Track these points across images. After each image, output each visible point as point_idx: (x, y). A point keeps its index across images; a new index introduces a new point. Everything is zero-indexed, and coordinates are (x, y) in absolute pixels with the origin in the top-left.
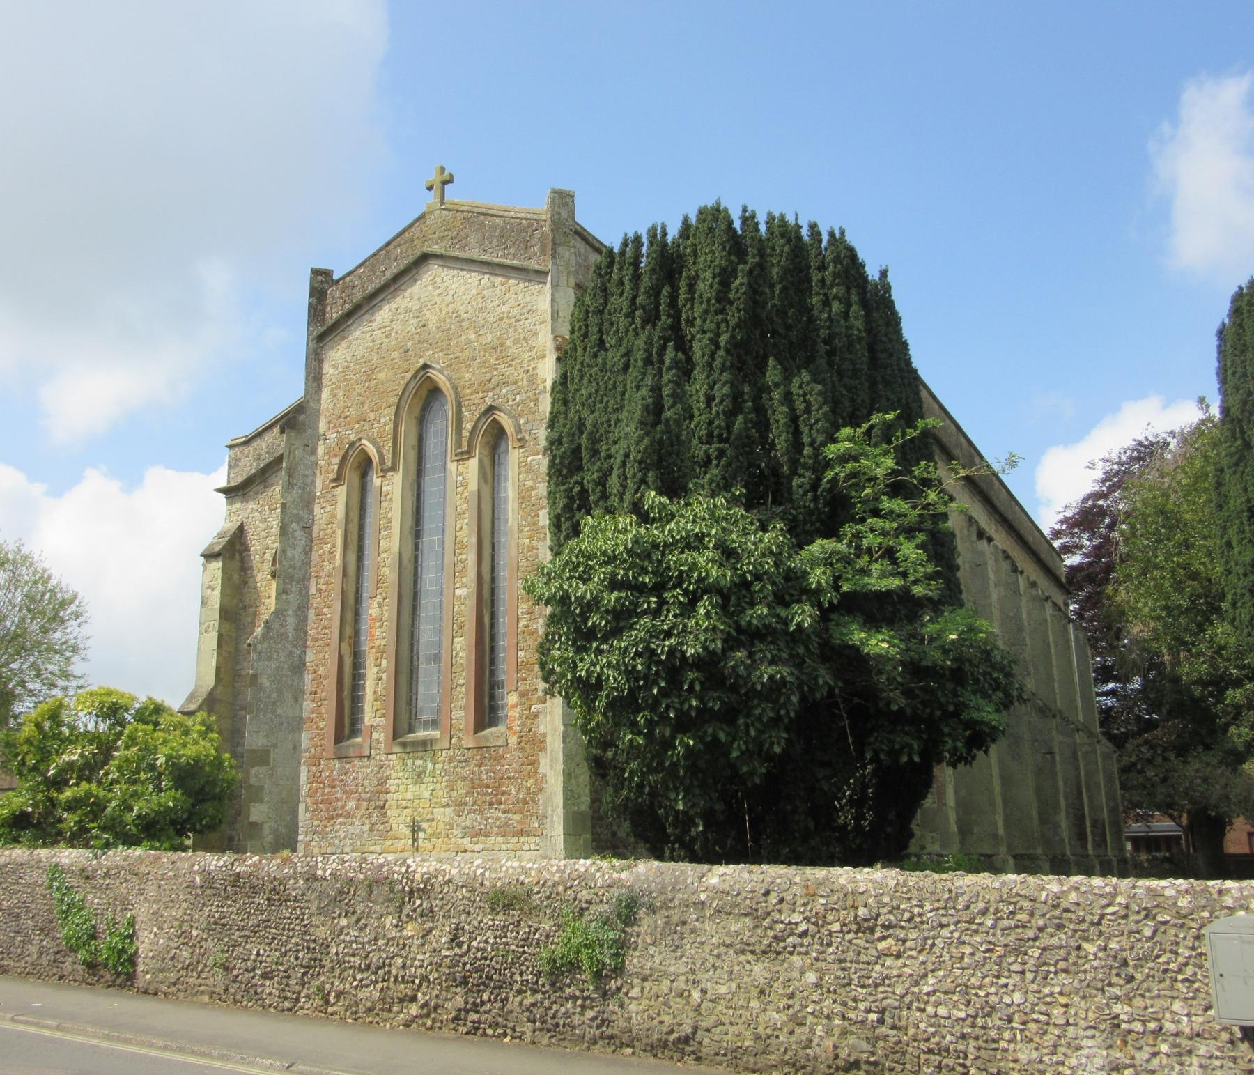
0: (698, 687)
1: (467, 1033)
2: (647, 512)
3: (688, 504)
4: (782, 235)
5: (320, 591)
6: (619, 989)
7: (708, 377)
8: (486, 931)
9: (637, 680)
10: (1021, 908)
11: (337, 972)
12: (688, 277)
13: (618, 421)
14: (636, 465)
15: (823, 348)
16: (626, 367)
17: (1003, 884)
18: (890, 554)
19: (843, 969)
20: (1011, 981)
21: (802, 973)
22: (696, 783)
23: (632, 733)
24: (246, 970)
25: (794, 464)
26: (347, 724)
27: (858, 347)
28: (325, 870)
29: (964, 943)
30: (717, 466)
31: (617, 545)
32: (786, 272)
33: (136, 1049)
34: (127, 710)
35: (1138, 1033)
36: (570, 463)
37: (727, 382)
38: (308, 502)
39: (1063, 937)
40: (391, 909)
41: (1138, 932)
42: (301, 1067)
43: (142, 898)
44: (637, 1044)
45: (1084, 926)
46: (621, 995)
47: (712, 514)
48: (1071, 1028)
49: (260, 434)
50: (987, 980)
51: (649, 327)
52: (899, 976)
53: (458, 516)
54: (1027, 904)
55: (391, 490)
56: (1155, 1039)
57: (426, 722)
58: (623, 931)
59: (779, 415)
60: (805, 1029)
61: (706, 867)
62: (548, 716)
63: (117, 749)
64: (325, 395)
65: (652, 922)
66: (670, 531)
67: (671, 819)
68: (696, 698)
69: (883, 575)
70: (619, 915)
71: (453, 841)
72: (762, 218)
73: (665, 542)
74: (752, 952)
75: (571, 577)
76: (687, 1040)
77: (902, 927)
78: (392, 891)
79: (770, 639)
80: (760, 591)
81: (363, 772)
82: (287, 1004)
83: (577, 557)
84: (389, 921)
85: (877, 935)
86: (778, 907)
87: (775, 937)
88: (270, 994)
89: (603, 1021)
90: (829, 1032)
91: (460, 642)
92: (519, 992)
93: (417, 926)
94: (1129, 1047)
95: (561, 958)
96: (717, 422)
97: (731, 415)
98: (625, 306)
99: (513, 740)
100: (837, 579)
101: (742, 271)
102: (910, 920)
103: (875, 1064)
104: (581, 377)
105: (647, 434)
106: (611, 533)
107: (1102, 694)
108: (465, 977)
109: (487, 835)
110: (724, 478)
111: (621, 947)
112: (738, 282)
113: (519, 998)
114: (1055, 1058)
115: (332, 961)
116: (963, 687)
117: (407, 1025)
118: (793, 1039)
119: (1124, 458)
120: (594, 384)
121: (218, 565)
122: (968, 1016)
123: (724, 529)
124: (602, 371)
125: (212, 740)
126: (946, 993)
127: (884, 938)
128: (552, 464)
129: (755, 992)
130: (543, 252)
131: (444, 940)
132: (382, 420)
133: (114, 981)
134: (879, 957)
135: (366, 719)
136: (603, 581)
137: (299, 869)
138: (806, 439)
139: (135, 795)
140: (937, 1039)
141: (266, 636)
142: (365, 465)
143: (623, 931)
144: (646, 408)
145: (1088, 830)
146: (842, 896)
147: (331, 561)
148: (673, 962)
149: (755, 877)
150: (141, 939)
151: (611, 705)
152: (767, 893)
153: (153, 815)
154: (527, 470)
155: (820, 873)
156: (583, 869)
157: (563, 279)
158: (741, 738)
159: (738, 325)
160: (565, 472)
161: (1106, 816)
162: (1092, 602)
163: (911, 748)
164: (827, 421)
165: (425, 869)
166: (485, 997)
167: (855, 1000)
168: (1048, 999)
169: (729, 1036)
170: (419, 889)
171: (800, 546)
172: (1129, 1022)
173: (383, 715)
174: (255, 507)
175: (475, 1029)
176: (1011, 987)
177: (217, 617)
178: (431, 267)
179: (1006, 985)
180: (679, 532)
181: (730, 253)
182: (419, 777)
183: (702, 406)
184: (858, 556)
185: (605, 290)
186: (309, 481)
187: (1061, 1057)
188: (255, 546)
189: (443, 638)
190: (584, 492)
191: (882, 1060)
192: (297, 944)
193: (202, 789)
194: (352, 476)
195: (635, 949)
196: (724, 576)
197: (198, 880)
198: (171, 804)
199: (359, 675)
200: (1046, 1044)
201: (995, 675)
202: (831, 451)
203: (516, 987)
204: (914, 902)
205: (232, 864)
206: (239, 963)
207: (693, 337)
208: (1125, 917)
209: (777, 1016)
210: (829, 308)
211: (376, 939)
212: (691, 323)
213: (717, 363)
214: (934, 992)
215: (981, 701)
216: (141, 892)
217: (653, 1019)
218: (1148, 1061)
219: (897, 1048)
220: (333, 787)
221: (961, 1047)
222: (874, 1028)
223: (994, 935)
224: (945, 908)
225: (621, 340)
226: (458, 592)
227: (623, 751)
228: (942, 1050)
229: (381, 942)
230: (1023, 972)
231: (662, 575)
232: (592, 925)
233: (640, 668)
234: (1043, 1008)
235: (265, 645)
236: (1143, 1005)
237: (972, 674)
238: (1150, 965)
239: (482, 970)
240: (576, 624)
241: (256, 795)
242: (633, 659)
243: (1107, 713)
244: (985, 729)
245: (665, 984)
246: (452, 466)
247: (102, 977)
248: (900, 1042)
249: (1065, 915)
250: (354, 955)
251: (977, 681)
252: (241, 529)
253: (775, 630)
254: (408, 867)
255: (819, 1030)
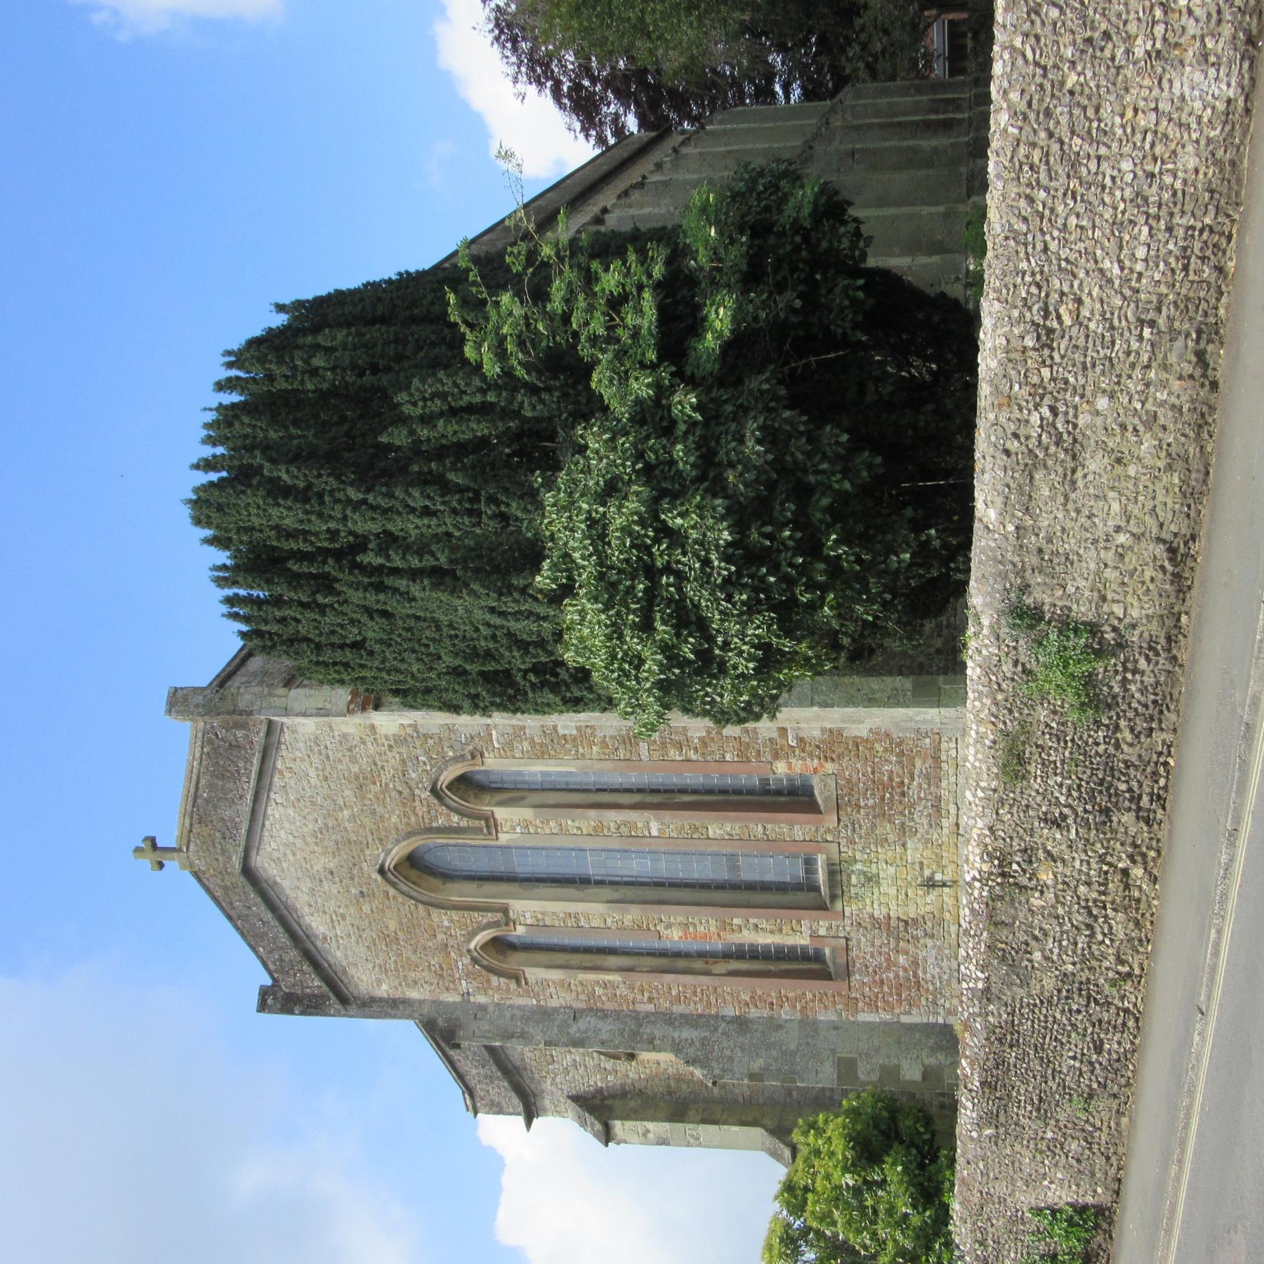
0: (769, 529)
1: (1164, 808)
2: (561, 586)
3: (552, 538)
4: (230, 425)
5: (650, 1000)
6: (1115, 629)
7: (399, 514)
8: (1049, 786)
9: (759, 602)
10: (1027, 157)
11: (1095, 963)
12: (278, 539)
13: (451, 625)
14: (503, 599)
15: (368, 379)
16: (385, 614)
17: (998, 176)
18: (616, 303)
19: (1094, 366)
20: (1109, 172)
21: (1098, 413)
22: (880, 537)
23: (822, 607)
24: (1092, 1072)
25: (506, 414)
26: (808, 965)
27: (368, 336)
28: (977, 979)
29: (1065, 225)
30: (508, 505)
31: (599, 623)
32: (274, 420)
33: (1183, 1195)
34: (789, 1225)
35: (1166, 30)
36: (500, 684)
37: (407, 492)
38: (544, 1015)
39: (1059, 109)
40: (1023, 899)
41: (1055, 24)
42: (1202, 998)
43: (1009, 1200)
44: (1176, 609)
45: (1048, 86)
46: (1121, 627)
47: (565, 508)
48: (1160, 106)
49: (460, 1077)
50: (1107, 200)
51: (337, 586)
52: (1102, 301)
53: (563, 831)
54: (1022, 150)
55: (530, 912)
56: (1173, 10)
57: (807, 871)
58: (1049, 623)
59: (449, 430)
60: (1160, 412)
61: (976, 525)
62: (803, 725)
63: (836, 1235)
64: (414, 994)
65: (1039, 589)
66: (583, 558)
67: (921, 571)
68: (782, 531)
69: (639, 312)
70: (1031, 627)
71: (945, 839)
72: (208, 451)
73: (597, 564)
74: (1074, 471)
75: (637, 678)
76: (1172, 551)
77: (1047, 295)
78: (1002, 898)
79: (713, 444)
80: (656, 453)
81: (865, 947)
82: (1131, 1023)
83: (613, 671)
84: (1036, 902)
85: (1055, 325)
86: (1022, 439)
87: (1057, 444)
88: (1119, 1043)
89: (1150, 648)
90: (1164, 385)
91: (714, 831)
92: (1117, 746)
93: (1042, 868)
94: (1182, 41)
95: (1079, 696)
96: (455, 504)
97: (447, 488)
98: (311, 615)
99: (830, 767)
100: (643, 366)
101: (271, 471)
102: (1039, 287)
103: (1199, 332)
104: (398, 671)
105: (467, 585)
106: (585, 631)
107: (787, 98)
108: (1101, 811)
109: (939, 798)
110: (522, 497)
111: (1067, 626)
112: (284, 476)
113: (1125, 747)
114: (1194, 126)
115: (1082, 970)
116: (773, 224)
117: (1155, 880)
118: (1171, 427)
119: (514, 59)
120: (406, 655)
121: (618, 1126)
122: (1146, 223)
123: (582, 495)
124: (390, 645)
125: (826, 1122)
126: (1121, 248)
127: (1059, 317)
128: (502, 707)
129: (1119, 469)
130: (243, 726)
131: (1058, 836)
132: (446, 923)
133: (1105, 1231)
134: (1081, 324)
135: (803, 942)
136: (642, 640)
137: (977, 1010)
138: (478, 399)
139: (891, 1211)
140: (1172, 260)
141: (704, 1064)
142: (500, 945)
143: (1049, 623)
144: (435, 586)
145: (941, 117)
146: (1010, 365)
147: (614, 986)
148: (1084, 564)
149: (988, 467)
150: (1056, 1200)
151: (788, 632)
152: (1007, 453)
153: (912, 1189)
154: (508, 740)
155: (984, 390)
156: (978, 670)
157: (277, 702)
158: (828, 478)
159: (338, 478)
160: (511, 692)
161: (925, 98)
162: (680, 102)
163: (843, 295)
164: (456, 374)
165: (978, 859)
166: (1123, 787)
167: (1128, 354)
168: (1129, 130)
169: (1168, 501)
170: (1000, 866)
171: (605, 409)
172: (1154, 40)
173: (799, 922)
174: (549, 1081)
175: (1159, 799)
176: (1115, 173)
177: (680, 1125)
178: (259, 864)
179: (1113, 178)
180: (585, 548)
181: (249, 485)
182: (871, 880)
183: (434, 522)
184: (618, 341)
185: (291, 641)
186: (518, 1013)
187: (1193, 120)
188: (596, 1081)
189: (709, 850)
190: (536, 669)
191: (1195, 324)
192: (1063, 1011)
193: (883, 1133)
194: (514, 961)
195: (1070, 609)
196: (637, 494)
197: (988, 1132)
198: (899, 1168)
199: (751, 951)
200: (1178, 135)
201: (761, 188)
202: (492, 368)
203: (1111, 750)
204: (1019, 280)
205: (970, 1091)
206: (1084, 1081)
207: (351, 533)
208: (1037, 38)
209: (1146, 445)
210: (321, 370)
211: (1057, 917)
212: (334, 534)
213: (384, 503)
214: (1119, 261)
215: (790, 205)
216: (1002, 1201)
217: (1148, 589)
218: (1197, 20)
219: (1182, 306)
220: (882, 982)
221: (1180, 232)
222: (1159, 332)
223: (1056, 190)
224: (1026, 245)
225: (352, 621)
226: (655, 833)
227: (842, 625)
228: (1185, 254)
229: (1060, 911)
230: (1099, 158)
231: (636, 570)
232: (1041, 660)
233: (744, 597)
234: (1139, 137)
235: (714, 1064)
236: (1135, 23)
237: (759, 213)
238: (1091, 12)
239: (1093, 790)
240: (690, 678)
241: (890, 1073)
242: (734, 605)
243: (808, 95)
244: (823, 199)
245: (1110, 574)
246: (504, 838)
247: (1100, 1245)
248: (1175, 303)
249: (1035, 106)
250: (1076, 944)
251: (767, 209)
252: (577, 1099)
253: (701, 437)
254: (974, 879)
255: (1162, 396)
